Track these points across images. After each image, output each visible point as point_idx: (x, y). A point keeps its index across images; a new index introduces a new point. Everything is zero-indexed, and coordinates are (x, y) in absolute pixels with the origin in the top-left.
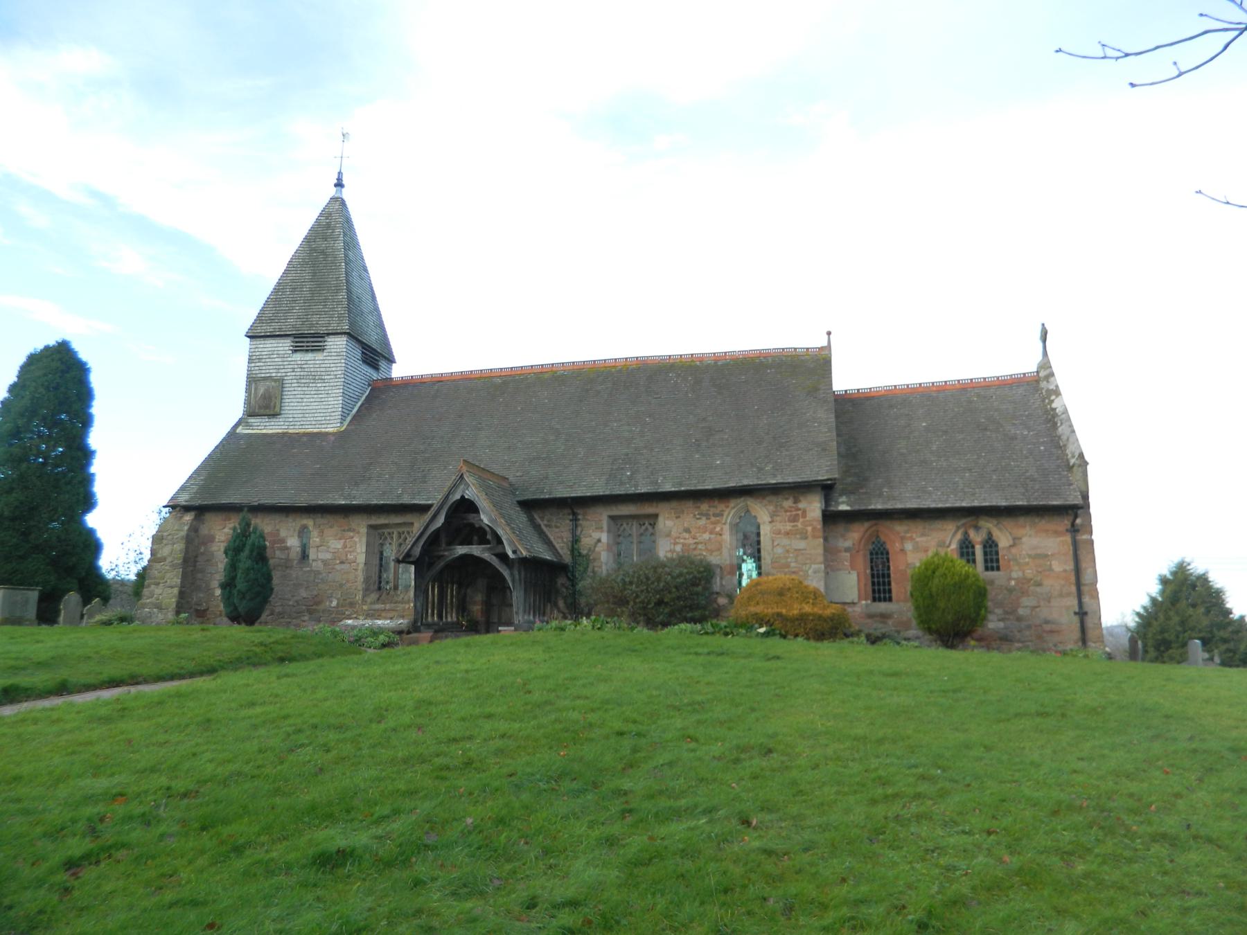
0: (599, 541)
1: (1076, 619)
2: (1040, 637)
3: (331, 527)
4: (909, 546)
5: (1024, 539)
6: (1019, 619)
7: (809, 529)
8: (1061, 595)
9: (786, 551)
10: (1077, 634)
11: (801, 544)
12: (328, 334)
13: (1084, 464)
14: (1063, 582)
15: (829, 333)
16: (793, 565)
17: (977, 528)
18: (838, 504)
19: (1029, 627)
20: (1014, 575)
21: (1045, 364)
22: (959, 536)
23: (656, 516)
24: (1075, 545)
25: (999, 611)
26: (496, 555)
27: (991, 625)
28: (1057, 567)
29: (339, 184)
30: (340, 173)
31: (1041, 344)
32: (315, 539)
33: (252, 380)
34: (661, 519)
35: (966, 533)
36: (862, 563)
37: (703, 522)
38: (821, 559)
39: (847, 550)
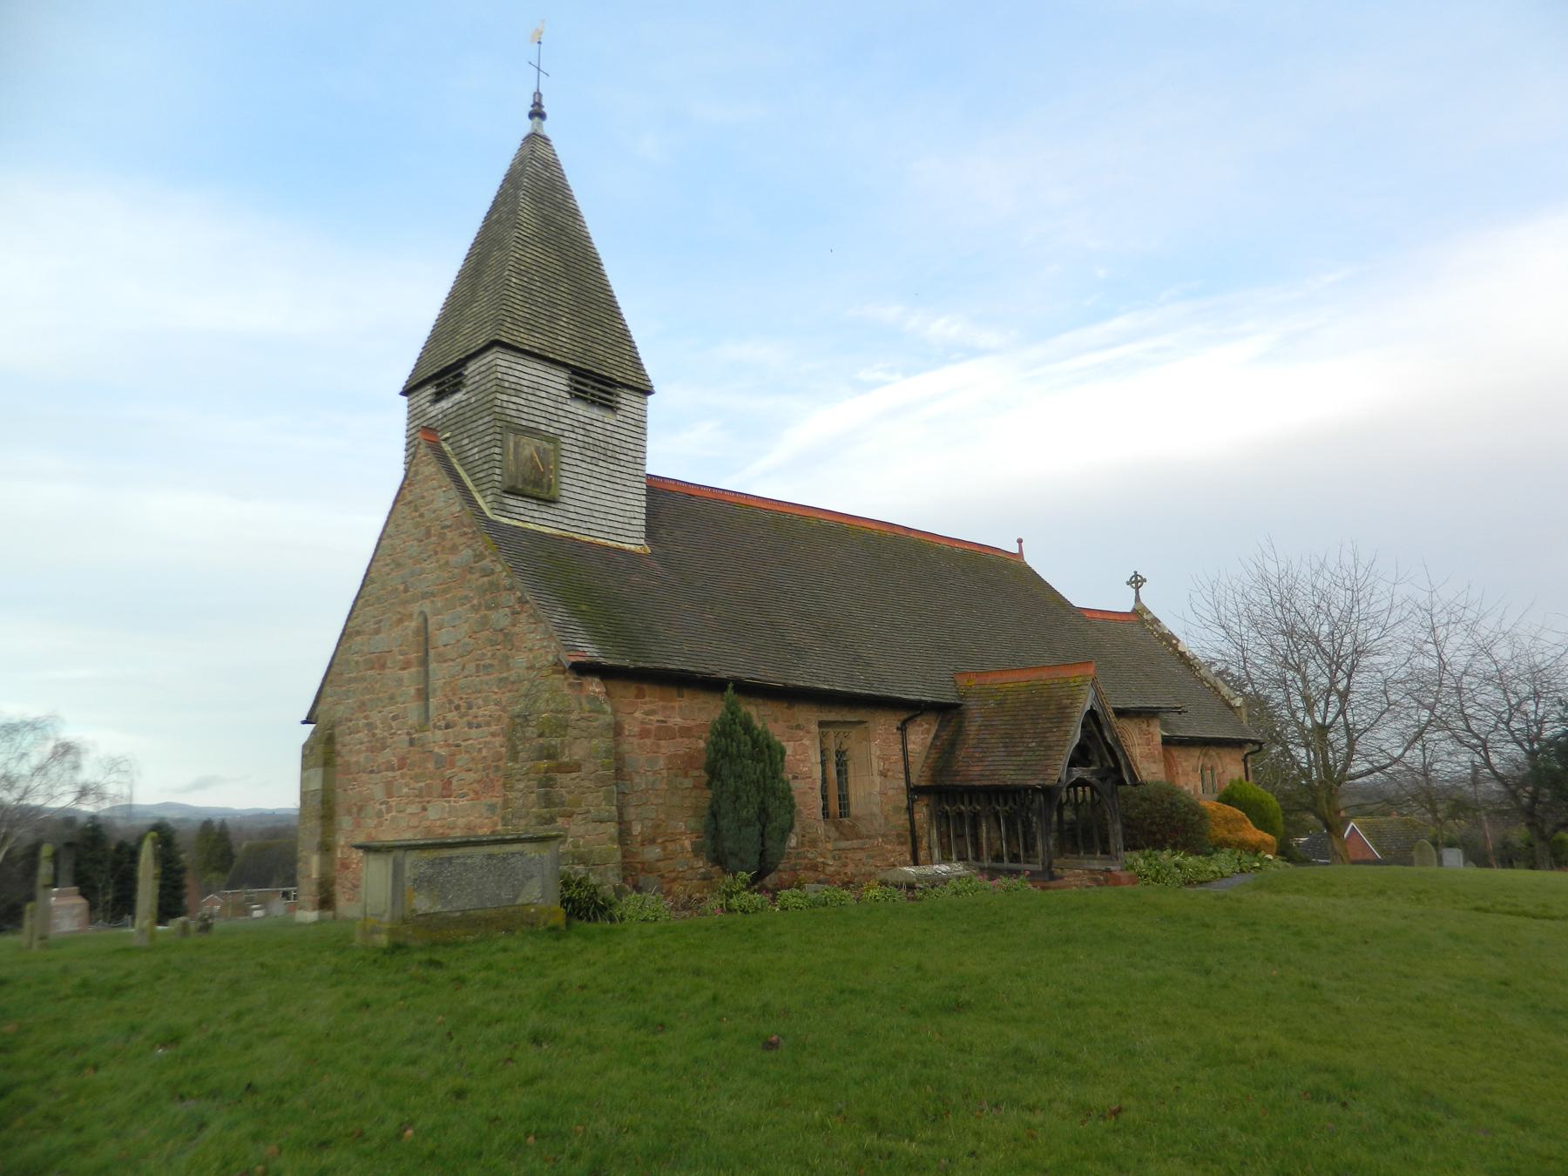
15: (1020, 541)
29: (537, 113)
30: (538, 94)
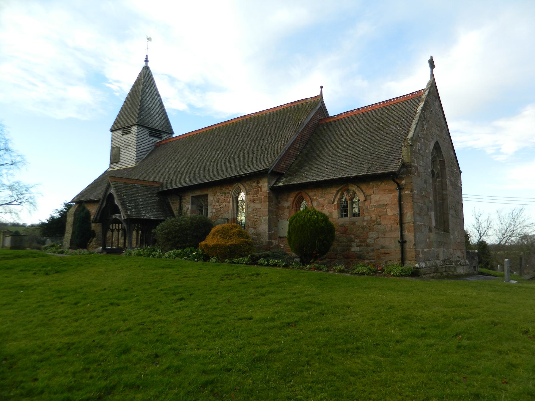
0: (188, 209)
1: (399, 245)
2: (378, 257)
5: (372, 196)
6: (368, 246)
7: (263, 197)
8: (391, 231)
10: (399, 256)
11: (258, 206)
12: (132, 126)
14: (392, 222)
15: (322, 87)
16: (255, 217)
19: (373, 250)
20: (366, 219)
23: (207, 195)
25: (357, 241)
27: (353, 249)
29: (146, 61)
30: (147, 56)
31: (429, 70)
33: (112, 149)
38: (267, 213)
39: (288, 208)
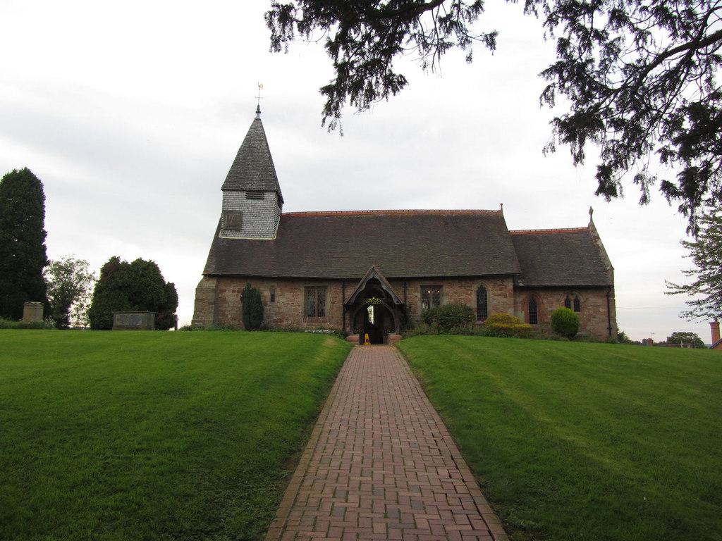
3: (286, 287)
4: (545, 301)
9: (502, 303)
11: (505, 300)
13: (612, 269)
17: (572, 294)
18: (519, 283)
21: (592, 224)
22: (565, 297)
23: (442, 286)
24: (608, 301)
26: (388, 303)
28: (601, 310)
29: (258, 112)
30: (258, 106)
32: (278, 292)
34: (444, 288)
35: (567, 297)
36: (527, 308)
37: (463, 289)
